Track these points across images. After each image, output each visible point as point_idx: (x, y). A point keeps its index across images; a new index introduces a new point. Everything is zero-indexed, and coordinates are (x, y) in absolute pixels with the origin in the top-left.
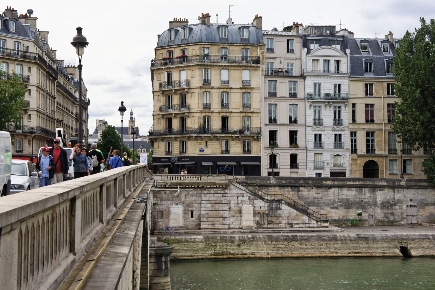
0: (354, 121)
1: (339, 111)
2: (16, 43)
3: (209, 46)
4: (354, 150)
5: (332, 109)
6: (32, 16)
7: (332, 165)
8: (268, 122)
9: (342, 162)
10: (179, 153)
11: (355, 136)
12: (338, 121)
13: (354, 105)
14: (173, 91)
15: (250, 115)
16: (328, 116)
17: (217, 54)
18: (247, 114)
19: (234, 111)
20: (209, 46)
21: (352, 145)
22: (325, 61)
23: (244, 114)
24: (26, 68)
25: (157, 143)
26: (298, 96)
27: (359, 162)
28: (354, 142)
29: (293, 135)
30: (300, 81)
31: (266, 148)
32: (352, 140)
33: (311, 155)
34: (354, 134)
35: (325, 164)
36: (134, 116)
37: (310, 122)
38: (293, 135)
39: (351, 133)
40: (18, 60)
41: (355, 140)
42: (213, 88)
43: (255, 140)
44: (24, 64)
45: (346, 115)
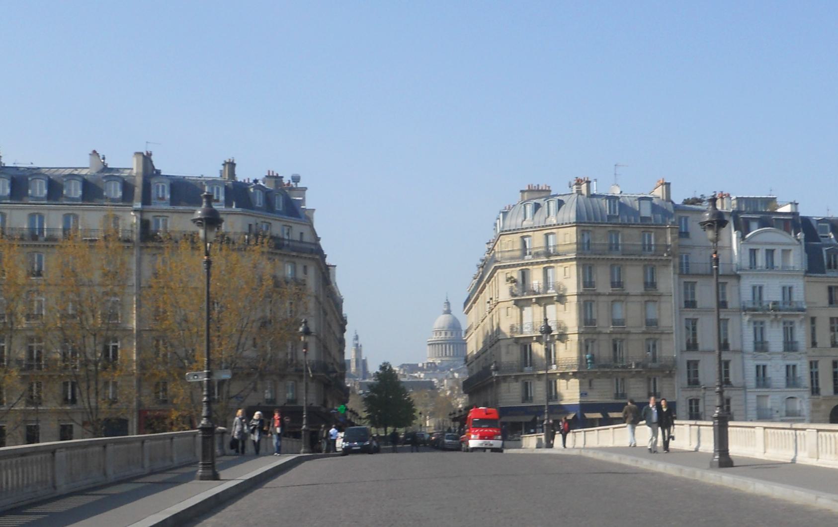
0: (814, 344)
1: (762, 329)
2: (286, 228)
3: (590, 229)
4: (815, 391)
5: (781, 325)
6: (300, 185)
7: (784, 413)
8: (685, 348)
9: (798, 408)
10: (520, 400)
11: (816, 367)
12: (790, 346)
13: (813, 320)
14: (534, 300)
15: (657, 336)
16: (775, 336)
17: (603, 242)
18: (652, 336)
19: (633, 330)
20: (590, 229)
21: (812, 381)
22: (783, 251)
23: (647, 336)
24: (300, 269)
25: (506, 384)
26: (729, 305)
27: (823, 407)
28: (814, 376)
29: (724, 366)
30: (731, 282)
31: (683, 389)
32: (812, 373)
33: (752, 398)
34: (813, 365)
35: (774, 412)
36: (360, 342)
37: (749, 345)
38: (724, 366)
39: (811, 363)
40: (289, 256)
41: (817, 373)
42: (599, 294)
43: (666, 376)
44: (296, 260)
45: (801, 335)
